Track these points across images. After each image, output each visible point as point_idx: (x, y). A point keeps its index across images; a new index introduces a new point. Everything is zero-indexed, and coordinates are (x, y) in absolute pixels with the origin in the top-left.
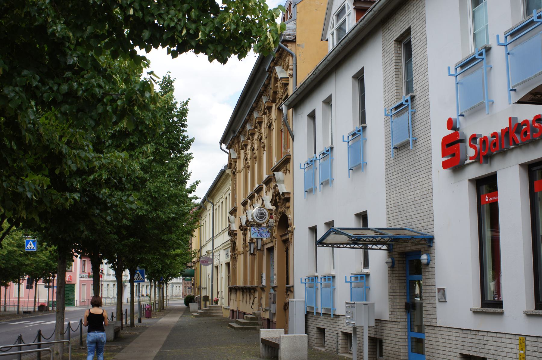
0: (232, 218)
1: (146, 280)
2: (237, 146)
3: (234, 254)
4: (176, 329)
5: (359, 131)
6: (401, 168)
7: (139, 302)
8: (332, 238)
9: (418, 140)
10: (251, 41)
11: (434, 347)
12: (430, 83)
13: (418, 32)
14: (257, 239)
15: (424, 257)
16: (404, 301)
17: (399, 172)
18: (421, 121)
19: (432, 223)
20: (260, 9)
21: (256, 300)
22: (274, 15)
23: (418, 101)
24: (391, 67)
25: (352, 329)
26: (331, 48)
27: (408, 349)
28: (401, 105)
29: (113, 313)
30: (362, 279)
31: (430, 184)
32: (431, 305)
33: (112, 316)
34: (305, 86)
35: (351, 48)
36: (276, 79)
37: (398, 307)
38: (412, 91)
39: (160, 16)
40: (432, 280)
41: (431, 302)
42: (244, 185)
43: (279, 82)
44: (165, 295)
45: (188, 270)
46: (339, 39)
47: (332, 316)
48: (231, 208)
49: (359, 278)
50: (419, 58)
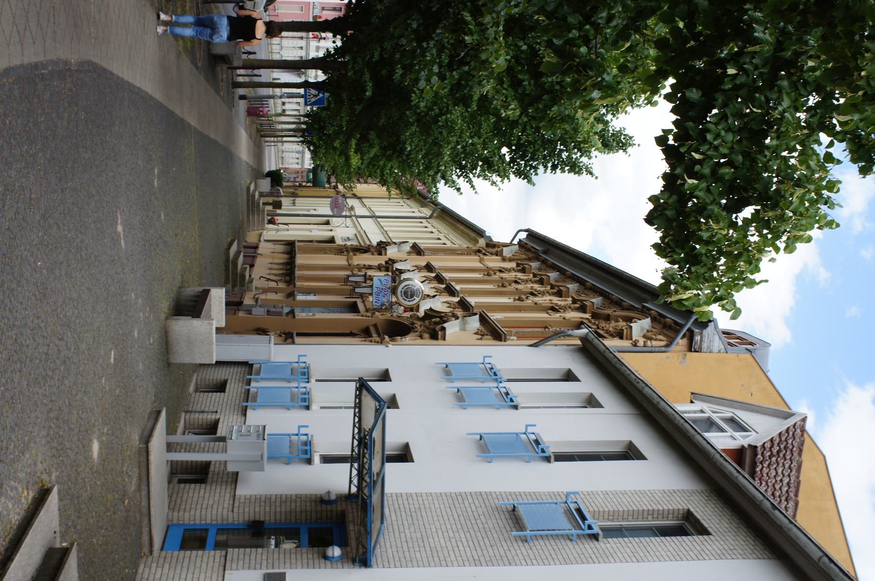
0: (407, 248)
1: (309, 108)
2: (523, 256)
3: (347, 251)
4: (228, 155)
5: (543, 451)
6: (482, 518)
7: (272, 97)
8: (369, 404)
9: (526, 545)
10: (682, 264)
11: (192, 565)
12: (619, 564)
13: (703, 547)
14: (372, 286)
15: (336, 551)
16: (267, 518)
17: (475, 513)
18: (557, 550)
19: (392, 565)
20: (735, 279)
21: (273, 285)
22: (725, 302)
23: (589, 546)
24: (646, 503)
25: (223, 435)
26: (679, 408)
27: (189, 525)
28: (584, 518)
29: (255, 53)
30: (304, 453)
31: (455, 563)
32: (259, 560)
33: (250, 53)
34: (618, 366)
35: (678, 439)
36: (629, 320)
37: (257, 510)
38: (605, 537)
39: (723, 117)
40: (299, 564)
41: (265, 563)
42: (459, 266)
43: (624, 324)
44: (285, 139)
45: (323, 176)
46: (695, 421)
47: (245, 404)
48: (422, 246)
49: (305, 448)
50: (660, 548)
